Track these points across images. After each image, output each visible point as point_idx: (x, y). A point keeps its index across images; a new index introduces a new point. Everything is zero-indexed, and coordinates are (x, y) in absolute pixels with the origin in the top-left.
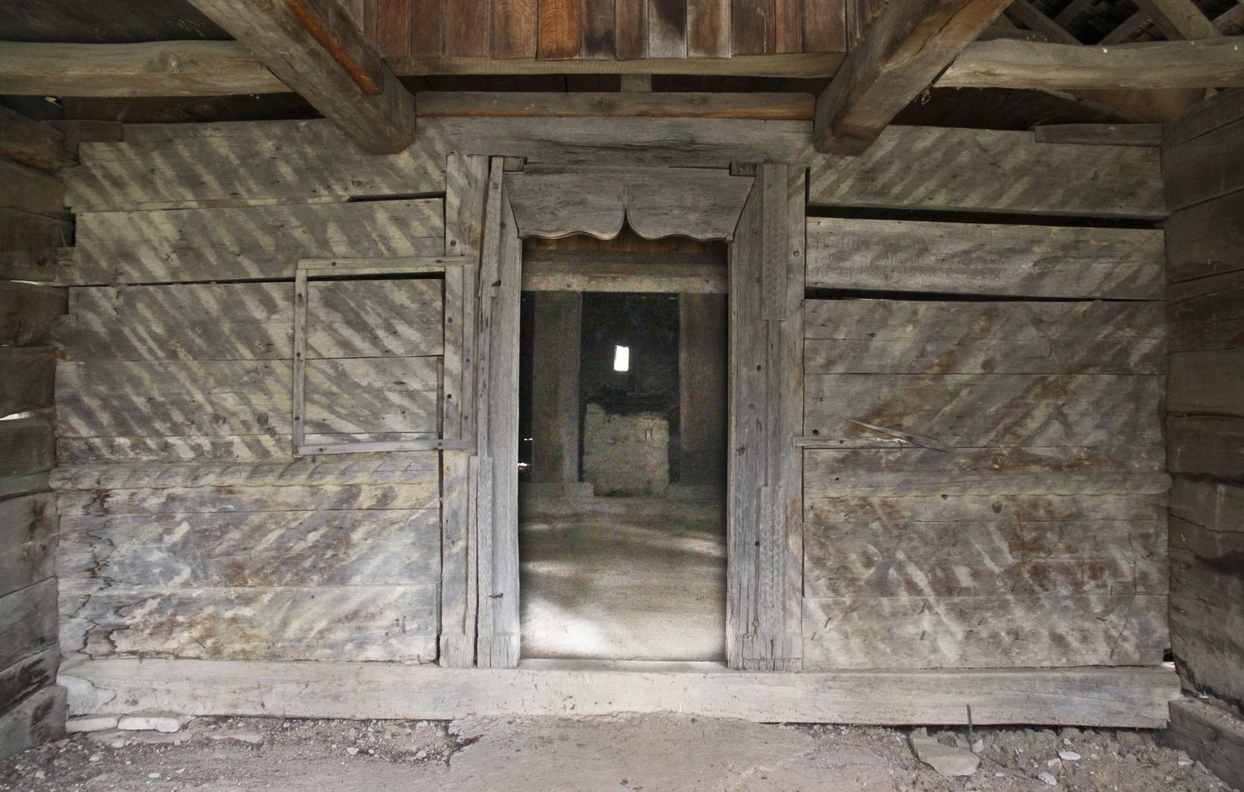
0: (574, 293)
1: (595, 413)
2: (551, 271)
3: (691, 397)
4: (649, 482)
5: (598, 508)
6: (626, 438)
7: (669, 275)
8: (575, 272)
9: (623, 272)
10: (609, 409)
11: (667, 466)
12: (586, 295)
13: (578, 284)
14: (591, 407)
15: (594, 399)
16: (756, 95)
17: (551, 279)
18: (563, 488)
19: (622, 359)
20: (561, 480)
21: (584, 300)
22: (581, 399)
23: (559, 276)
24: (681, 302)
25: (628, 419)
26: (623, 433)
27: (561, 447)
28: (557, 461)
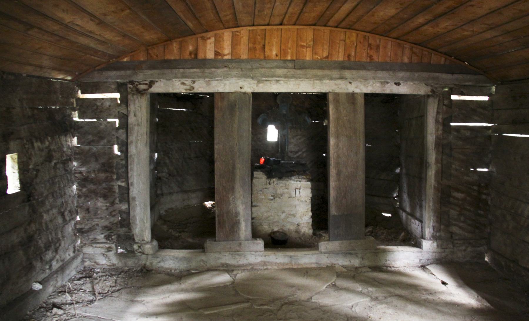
0: (245, 93)
1: (260, 177)
2: (226, 76)
3: (339, 174)
4: (298, 225)
5: (267, 259)
6: (281, 195)
7: (321, 78)
8: (246, 76)
9: (286, 77)
10: (270, 175)
11: (310, 214)
12: (256, 96)
13: (250, 86)
14: (258, 174)
15: (260, 168)
16: (215, 126)
17: (227, 82)
18: (240, 244)
19: (272, 134)
20: (239, 237)
21: (365, 99)
22: (252, 169)
23: (233, 80)
24: (331, 98)
25: (284, 182)
26: (280, 191)
27: (237, 214)
28: (235, 224)
